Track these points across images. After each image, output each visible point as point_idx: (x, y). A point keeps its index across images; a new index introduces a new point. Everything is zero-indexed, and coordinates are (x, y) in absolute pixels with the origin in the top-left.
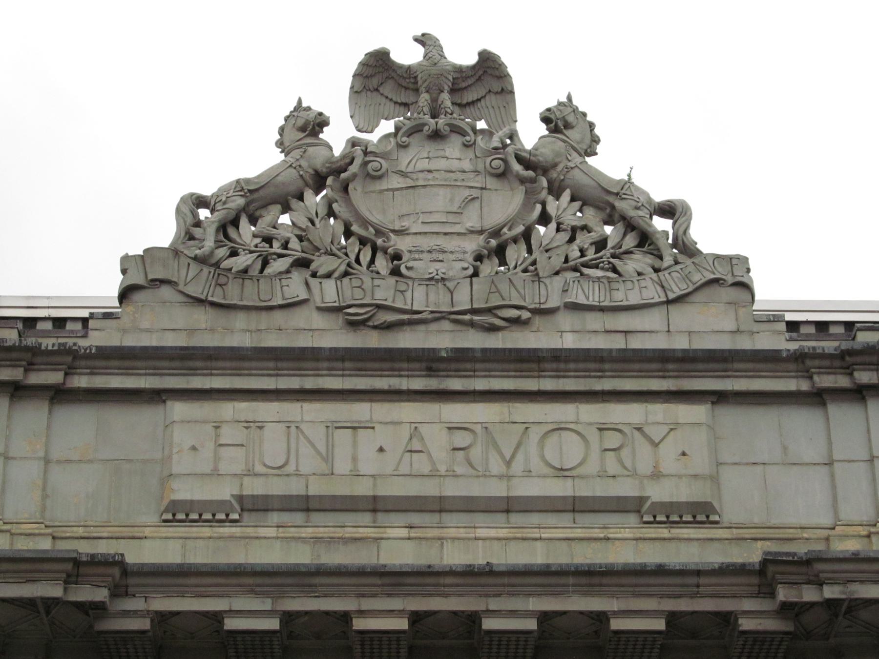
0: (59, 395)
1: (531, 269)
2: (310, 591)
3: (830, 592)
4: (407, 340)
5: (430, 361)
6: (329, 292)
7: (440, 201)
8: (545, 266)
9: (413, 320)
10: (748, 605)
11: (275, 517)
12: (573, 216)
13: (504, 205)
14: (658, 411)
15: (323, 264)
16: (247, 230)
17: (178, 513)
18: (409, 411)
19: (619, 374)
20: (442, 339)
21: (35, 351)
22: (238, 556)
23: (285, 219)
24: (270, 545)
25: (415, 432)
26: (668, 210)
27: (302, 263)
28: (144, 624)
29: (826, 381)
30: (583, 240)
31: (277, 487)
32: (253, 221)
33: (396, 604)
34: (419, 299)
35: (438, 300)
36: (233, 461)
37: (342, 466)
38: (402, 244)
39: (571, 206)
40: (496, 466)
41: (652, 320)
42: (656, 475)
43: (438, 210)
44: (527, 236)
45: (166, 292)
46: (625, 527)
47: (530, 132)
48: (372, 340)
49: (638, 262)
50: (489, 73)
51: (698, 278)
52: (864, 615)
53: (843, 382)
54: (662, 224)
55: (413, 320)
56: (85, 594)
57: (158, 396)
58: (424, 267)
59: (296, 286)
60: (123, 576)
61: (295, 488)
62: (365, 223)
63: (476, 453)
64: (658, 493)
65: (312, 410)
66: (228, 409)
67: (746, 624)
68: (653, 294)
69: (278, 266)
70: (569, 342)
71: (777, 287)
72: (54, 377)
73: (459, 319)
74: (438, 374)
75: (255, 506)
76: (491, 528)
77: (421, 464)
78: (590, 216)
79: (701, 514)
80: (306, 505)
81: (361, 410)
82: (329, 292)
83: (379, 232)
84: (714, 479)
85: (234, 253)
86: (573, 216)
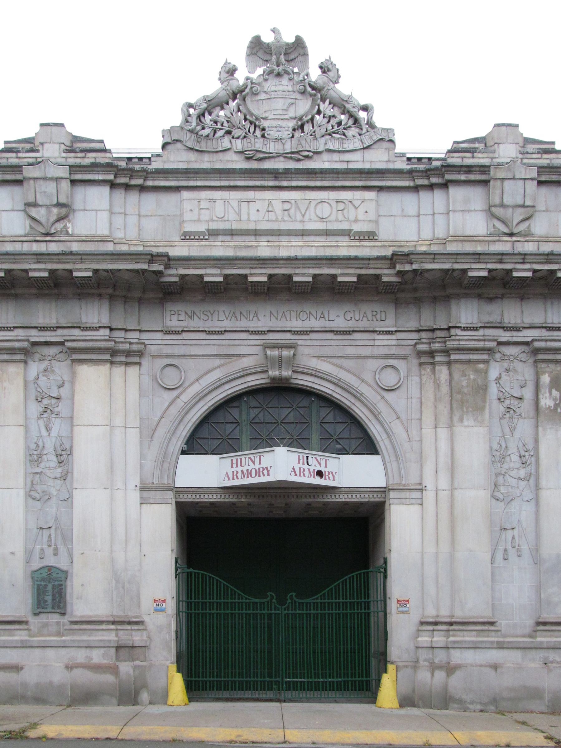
0: (142, 189)
2: (234, 266)
3: (415, 267)
4: (268, 165)
5: (275, 174)
6: (239, 145)
7: (279, 105)
9: (270, 157)
11: (220, 238)
13: (303, 106)
14: (358, 194)
15: (237, 132)
16: (208, 118)
17: (187, 236)
20: (280, 165)
21: (132, 170)
23: (222, 113)
24: (220, 249)
25: (270, 204)
26: (365, 108)
27: (229, 133)
28: (176, 279)
29: (420, 182)
30: (333, 121)
31: (221, 226)
33: (263, 271)
34: (272, 148)
36: (205, 215)
37: (244, 217)
38: (265, 124)
39: (333, 110)
40: (299, 217)
42: (356, 221)
43: (279, 107)
44: (312, 120)
45: (179, 145)
46: (344, 241)
47: (315, 74)
48: (254, 165)
49: (353, 131)
50: (299, 44)
51: (375, 138)
53: (426, 182)
54: (363, 115)
55: (270, 157)
57: (177, 189)
59: (226, 143)
61: (227, 226)
62: (252, 115)
64: (357, 228)
66: (204, 194)
67: (385, 279)
68: (358, 145)
69: (220, 133)
70: (327, 166)
72: (140, 182)
73: (286, 156)
74: (278, 179)
75: (213, 233)
76: (297, 241)
77: (272, 216)
78: (336, 111)
81: (250, 194)
82: (239, 145)
83: (257, 119)
84: (377, 222)
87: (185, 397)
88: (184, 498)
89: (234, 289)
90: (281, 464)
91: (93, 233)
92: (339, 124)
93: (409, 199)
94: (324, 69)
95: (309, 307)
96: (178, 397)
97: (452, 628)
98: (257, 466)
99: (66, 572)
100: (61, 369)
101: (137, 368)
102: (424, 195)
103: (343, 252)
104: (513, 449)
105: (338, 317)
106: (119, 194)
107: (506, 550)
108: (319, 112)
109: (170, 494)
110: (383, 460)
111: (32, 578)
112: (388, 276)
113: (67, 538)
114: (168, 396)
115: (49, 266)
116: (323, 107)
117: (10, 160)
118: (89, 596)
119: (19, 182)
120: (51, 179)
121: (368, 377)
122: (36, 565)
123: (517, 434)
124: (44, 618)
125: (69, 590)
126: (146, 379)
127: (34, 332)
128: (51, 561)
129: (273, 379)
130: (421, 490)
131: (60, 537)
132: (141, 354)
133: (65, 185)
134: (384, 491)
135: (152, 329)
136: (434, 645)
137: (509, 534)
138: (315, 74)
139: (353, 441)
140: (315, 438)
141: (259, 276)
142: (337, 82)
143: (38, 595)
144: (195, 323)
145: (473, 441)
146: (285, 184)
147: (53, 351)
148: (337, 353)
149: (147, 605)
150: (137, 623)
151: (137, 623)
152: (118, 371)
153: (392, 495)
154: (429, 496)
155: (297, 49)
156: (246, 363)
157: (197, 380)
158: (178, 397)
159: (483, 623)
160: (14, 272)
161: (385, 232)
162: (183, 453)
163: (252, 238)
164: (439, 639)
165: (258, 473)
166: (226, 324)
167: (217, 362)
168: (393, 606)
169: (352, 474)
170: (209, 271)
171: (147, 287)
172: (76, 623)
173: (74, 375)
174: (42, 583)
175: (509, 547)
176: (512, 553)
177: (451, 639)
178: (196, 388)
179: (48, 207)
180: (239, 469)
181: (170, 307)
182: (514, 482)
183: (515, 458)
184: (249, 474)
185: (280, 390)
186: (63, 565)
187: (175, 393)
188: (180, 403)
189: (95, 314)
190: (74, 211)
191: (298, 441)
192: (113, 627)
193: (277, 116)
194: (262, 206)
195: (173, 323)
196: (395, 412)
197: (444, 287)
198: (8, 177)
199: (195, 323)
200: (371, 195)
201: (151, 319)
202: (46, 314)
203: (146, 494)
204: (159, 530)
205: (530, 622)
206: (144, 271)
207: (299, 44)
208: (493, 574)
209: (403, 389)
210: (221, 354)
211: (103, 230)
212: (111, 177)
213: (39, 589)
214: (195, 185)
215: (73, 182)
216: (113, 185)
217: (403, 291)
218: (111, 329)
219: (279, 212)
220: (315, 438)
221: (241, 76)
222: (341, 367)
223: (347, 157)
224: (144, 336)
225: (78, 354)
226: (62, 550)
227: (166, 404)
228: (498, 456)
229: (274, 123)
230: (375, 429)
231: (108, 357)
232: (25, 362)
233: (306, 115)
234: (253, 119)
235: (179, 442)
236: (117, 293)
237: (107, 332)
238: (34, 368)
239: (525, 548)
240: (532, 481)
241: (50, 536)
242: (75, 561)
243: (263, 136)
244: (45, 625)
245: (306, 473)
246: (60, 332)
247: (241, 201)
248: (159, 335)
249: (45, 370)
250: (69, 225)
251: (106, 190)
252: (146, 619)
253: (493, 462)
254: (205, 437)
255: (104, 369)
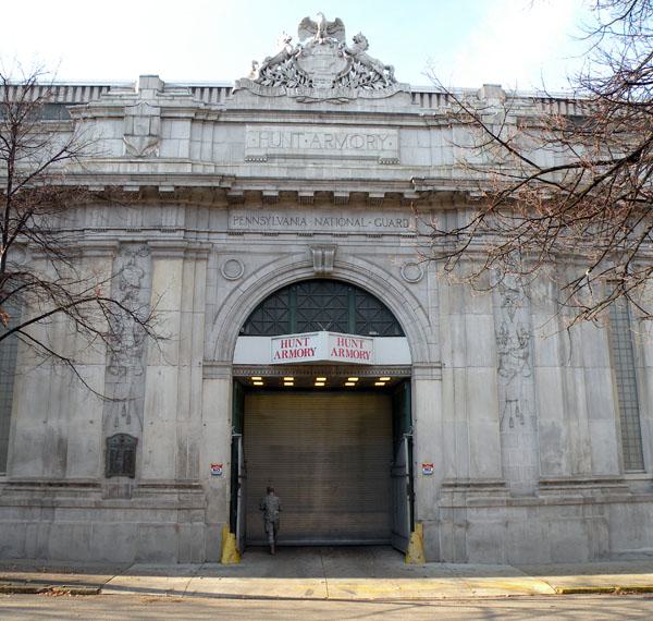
0: (216, 122)
1: (349, 86)
2: (286, 184)
3: (429, 188)
4: (314, 108)
5: (320, 114)
6: (292, 92)
7: (324, 64)
8: (353, 85)
9: (316, 101)
10: (407, 191)
11: (276, 160)
12: (360, 69)
13: (342, 65)
14: (384, 131)
15: (291, 84)
16: (269, 71)
17: (251, 160)
18: (315, 129)
19: (373, 119)
20: (323, 107)
21: (209, 110)
22: (266, 174)
23: (279, 68)
24: (276, 171)
25: (316, 136)
26: (388, 68)
27: (284, 83)
28: (241, 194)
29: (430, 123)
30: (364, 77)
31: (277, 152)
32: (270, 68)
33: (311, 189)
34: (317, 95)
35: (324, 96)
36: (265, 143)
37: (295, 145)
38: (313, 78)
39: (363, 70)
40: (338, 147)
41: (383, 102)
42: (383, 150)
43: (323, 66)
44: (348, 75)
45: (245, 91)
46: (374, 165)
47: (350, 45)
48: (305, 107)
49: (379, 85)
50: (338, 23)
51: (395, 90)
52: (439, 194)
53: (435, 123)
54: (386, 72)
55: (316, 101)
56: (225, 185)
57: (244, 123)
58: (319, 85)
59: (282, 90)
60: (235, 179)
61: (282, 152)
62: (302, 71)
63: (332, 143)
64: (383, 155)
65: (287, 128)
66: (264, 128)
67: (406, 196)
68: (383, 95)
69: (277, 84)
70: (359, 109)
71: (411, 75)
72: (215, 118)
73: (328, 100)
74: (322, 118)
75: (270, 157)
76: (337, 164)
77: (317, 145)
78: (366, 70)
79: (394, 162)
80: (285, 157)
81: (301, 129)
82: (292, 92)
83: (306, 73)
84: (399, 151)
85: (560, 465)
86: (360, 69)
87: (244, 287)
88: (241, 374)
89: (288, 200)
90: (322, 346)
91: (176, 156)
92: (369, 79)
93: (423, 134)
94: (356, 41)
95: (346, 215)
96: (238, 287)
97: (468, 489)
98: (303, 347)
99: (137, 439)
100: (143, 262)
101: (205, 263)
102: (436, 133)
103: (374, 175)
104: (512, 334)
105: (371, 222)
106: (198, 126)
107: (511, 419)
108: (353, 70)
109: (229, 370)
110: (409, 341)
111: (107, 444)
112: (409, 194)
113: (139, 411)
114: (230, 286)
115: (140, 183)
116: (356, 66)
117: (115, 102)
118: (156, 461)
119: (122, 117)
120: (147, 116)
121: (394, 272)
122: (111, 433)
123: (515, 319)
124: (114, 481)
125: (138, 457)
126: (213, 274)
127: (123, 233)
128: (124, 429)
129: (318, 273)
130: (441, 368)
131: (133, 409)
132: (209, 251)
133: (156, 121)
134: (410, 368)
135: (219, 230)
136: (455, 505)
137: (514, 405)
138: (350, 45)
139: (371, 312)
140: (352, 323)
141: (308, 192)
142: (366, 49)
143: (111, 460)
144: (254, 226)
145: (479, 323)
146: (327, 121)
147: (137, 248)
148: (379, 255)
149: (205, 469)
150: (196, 487)
151: (196, 487)
152: (190, 265)
153: (417, 371)
154: (448, 372)
155: (335, 28)
156: (296, 259)
157: (254, 273)
158: (238, 287)
159: (495, 485)
160: (195, 190)
161: (408, 158)
162: (241, 334)
163: (301, 161)
164: (458, 500)
165: (305, 353)
166: (279, 228)
167: (271, 258)
168: (419, 470)
169: (385, 353)
170: (267, 188)
171: (224, 197)
172: (143, 486)
173: (152, 267)
174: (116, 449)
175: (514, 416)
176: (516, 420)
177: (469, 499)
178: (253, 280)
179: (143, 137)
180: (288, 349)
181: (235, 213)
182: (514, 360)
183: (515, 340)
184: (296, 353)
185: (323, 282)
186: (134, 433)
187: (236, 283)
188: (239, 292)
189: (173, 218)
190: (162, 139)
191: (337, 327)
192: (175, 490)
193: (320, 75)
194: (310, 138)
195: (236, 226)
196: (417, 301)
197: (453, 202)
198: (113, 114)
199: (254, 226)
200: (393, 131)
201: (218, 222)
202: (133, 218)
203: (208, 371)
204: (219, 394)
205: (534, 482)
206: (215, 187)
207: (338, 23)
208: (502, 441)
209: (424, 281)
210: (271, 254)
211: (183, 153)
212: (193, 115)
213: (112, 454)
214: (266, 175)
215: (163, 118)
216: (193, 120)
217: (422, 204)
218: (186, 231)
219: (323, 143)
220: (352, 323)
221: (294, 43)
222: (372, 264)
223: (374, 103)
224: (213, 236)
225: (153, 251)
226: (135, 420)
227: (228, 293)
228: (501, 338)
229: (319, 77)
230: (401, 316)
231: (182, 254)
232: (114, 259)
233: (344, 72)
234: (303, 74)
235: (238, 327)
236: (192, 202)
237: (182, 233)
238: (122, 261)
239: (527, 416)
240: (530, 358)
241: (124, 407)
242: (145, 430)
243: (311, 86)
244: (116, 488)
245: (345, 353)
246: (143, 233)
247: (293, 134)
248: (224, 236)
249: (130, 264)
250: (157, 150)
251: (188, 124)
252: (204, 483)
253: (498, 343)
254: (260, 321)
255: (178, 263)
